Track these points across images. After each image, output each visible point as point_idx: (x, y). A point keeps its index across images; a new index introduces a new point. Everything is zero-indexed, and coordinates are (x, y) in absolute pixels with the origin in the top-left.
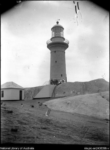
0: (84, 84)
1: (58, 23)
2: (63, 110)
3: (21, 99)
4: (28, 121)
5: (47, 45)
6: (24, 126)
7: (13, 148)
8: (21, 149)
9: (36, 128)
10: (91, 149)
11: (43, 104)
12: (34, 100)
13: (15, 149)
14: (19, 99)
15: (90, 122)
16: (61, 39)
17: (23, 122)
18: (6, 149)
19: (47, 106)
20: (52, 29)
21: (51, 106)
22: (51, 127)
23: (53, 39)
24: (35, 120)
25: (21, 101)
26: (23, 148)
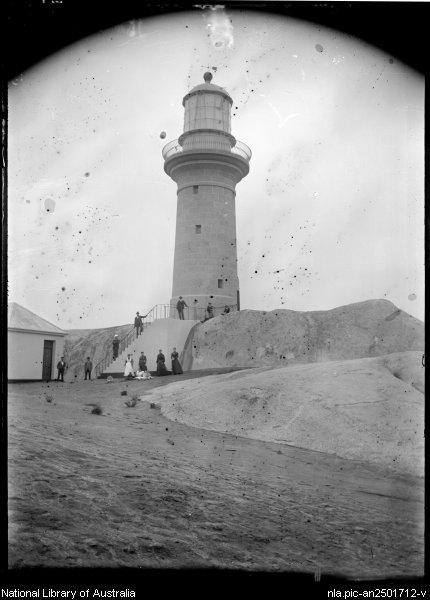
0: (312, 322)
1: (208, 77)
2: (232, 427)
3: (47, 377)
4: (72, 505)
5: (163, 162)
6: (44, 541)
7: (54, 594)
8: (82, 594)
9: (111, 551)
10: (356, 594)
11: (144, 398)
12: (102, 381)
13: (60, 594)
14: (40, 377)
15: (368, 498)
16: (221, 139)
17: (39, 512)
18: (22, 594)
19: (163, 410)
20: (185, 99)
21: (180, 409)
22: (194, 536)
23: (189, 139)
24: (106, 494)
25: (45, 384)
26: (91, 593)
